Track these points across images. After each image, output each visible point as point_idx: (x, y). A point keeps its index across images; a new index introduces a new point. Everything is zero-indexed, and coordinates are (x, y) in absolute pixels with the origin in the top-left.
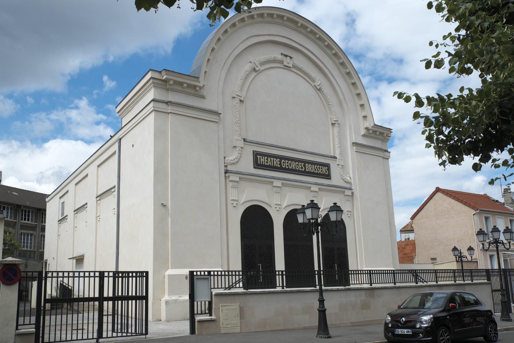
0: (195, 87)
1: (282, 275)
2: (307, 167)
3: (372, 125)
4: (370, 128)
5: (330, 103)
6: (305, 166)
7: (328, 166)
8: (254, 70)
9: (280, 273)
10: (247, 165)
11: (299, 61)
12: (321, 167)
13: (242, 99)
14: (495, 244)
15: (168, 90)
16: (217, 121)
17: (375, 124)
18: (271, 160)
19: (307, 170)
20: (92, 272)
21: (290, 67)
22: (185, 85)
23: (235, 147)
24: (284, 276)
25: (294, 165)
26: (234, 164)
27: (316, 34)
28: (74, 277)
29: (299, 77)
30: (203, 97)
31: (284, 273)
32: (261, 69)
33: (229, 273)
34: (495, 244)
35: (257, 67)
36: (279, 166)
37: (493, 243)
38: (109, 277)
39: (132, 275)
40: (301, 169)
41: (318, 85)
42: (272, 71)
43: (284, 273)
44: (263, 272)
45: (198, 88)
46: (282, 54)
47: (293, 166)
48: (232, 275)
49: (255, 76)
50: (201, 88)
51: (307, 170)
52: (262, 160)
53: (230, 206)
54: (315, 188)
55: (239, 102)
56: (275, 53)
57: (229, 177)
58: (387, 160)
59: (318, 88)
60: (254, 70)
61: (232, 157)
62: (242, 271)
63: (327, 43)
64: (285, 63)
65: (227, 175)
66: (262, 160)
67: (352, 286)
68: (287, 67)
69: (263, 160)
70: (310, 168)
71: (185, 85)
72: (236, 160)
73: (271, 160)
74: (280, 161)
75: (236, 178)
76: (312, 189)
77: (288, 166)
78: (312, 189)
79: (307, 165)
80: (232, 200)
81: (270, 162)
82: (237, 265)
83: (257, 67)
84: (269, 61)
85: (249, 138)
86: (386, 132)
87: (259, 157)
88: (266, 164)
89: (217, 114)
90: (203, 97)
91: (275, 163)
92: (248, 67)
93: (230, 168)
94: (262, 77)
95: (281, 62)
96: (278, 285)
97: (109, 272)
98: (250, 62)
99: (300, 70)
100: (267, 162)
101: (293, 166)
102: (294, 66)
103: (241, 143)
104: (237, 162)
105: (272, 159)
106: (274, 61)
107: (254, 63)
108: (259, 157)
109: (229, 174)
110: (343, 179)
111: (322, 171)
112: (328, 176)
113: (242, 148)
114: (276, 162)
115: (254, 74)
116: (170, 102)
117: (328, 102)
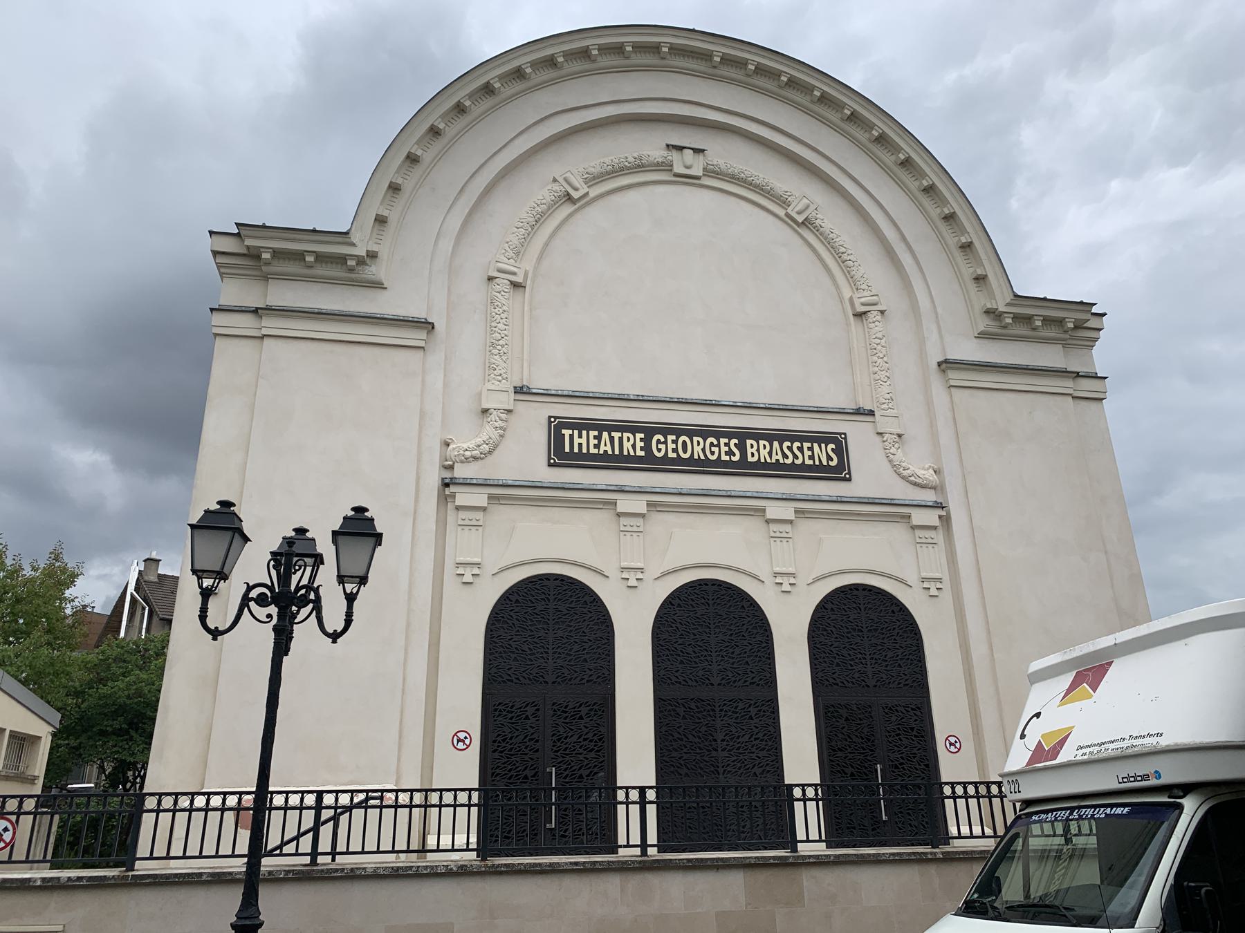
0: (342, 260)
1: (643, 802)
2: (749, 450)
3: (1009, 298)
4: (1002, 308)
5: (845, 257)
6: (742, 447)
7: (839, 443)
8: (569, 198)
9: (634, 795)
10: (525, 456)
11: (724, 153)
12: (806, 445)
13: (519, 279)
14: (273, 610)
15: (266, 278)
16: (422, 344)
17: (1016, 296)
18: (612, 439)
19: (750, 459)
20: (970, 783)
21: (698, 178)
22: (310, 259)
23: (485, 411)
24: (651, 810)
25: (697, 448)
26: (475, 458)
27: (778, 74)
28: (426, 806)
29: (733, 199)
30: (378, 285)
31: (651, 795)
32: (592, 195)
33: (427, 799)
34: (273, 610)
35: (576, 189)
36: (641, 453)
37: (262, 601)
38: (627, 803)
39: (989, 791)
40: (725, 458)
41: (799, 213)
42: (632, 195)
43: (651, 795)
44: (890, 789)
45: (351, 263)
46: (668, 146)
47: (698, 449)
48: (990, 796)
49: (571, 215)
50: (361, 261)
51: (750, 459)
52: (577, 441)
53: (451, 585)
54: (637, 504)
55: (508, 288)
56: (650, 144)
57: (453, 496)
58: (1093, 406)
59: (800, 219)
60: (569, 198)
61: (466, 442)
62: (658, 788)
63: (817, 93)
64: (679, 169)
65: (447, 491)
66: (582, 441)
67: (142, 868)
68: (688, 179)
69: (584, 441)
70: (764, 453)
71: (310, 259)
72: (486, 448)
73: (612, 439)
74: (647, 441)
75: (478, 498)
76: (770, 514)
77: (675, 450)
78: (770, 514)
79: (749, 442)
80: (459, 565)
81: (596, 446)
82: (463, 769)
83: (576, 189)
84: (622, 169)
85: (538, 384)
86: (1070, 318)
87: (567, 432)
88: (593, 451)
89: (428, 326)
90: (378, 285)
91: (627, 446)
92: (545, 194)
93: (461, 472)
94: (595, 216)
95: (666, 167)
96: (622, 840)
97: (803, 786)
98: (555, 180)
99: (734, 179)
100: (597, 446)
101: (698, 449)
102: (710, 172)
103: (507, 400)
104: (490, 452)
105: (616, 435)
106: (640, 167)
107: (566, 180)
108: (567, 432)
109: (453, 489)
110: (903, 478)
111: (812, 457)
112: (840, 471)
113: (509, 411)
114: (632, 444)
115: (567, 209)
116: (268, 309)
117: (838, 256)
